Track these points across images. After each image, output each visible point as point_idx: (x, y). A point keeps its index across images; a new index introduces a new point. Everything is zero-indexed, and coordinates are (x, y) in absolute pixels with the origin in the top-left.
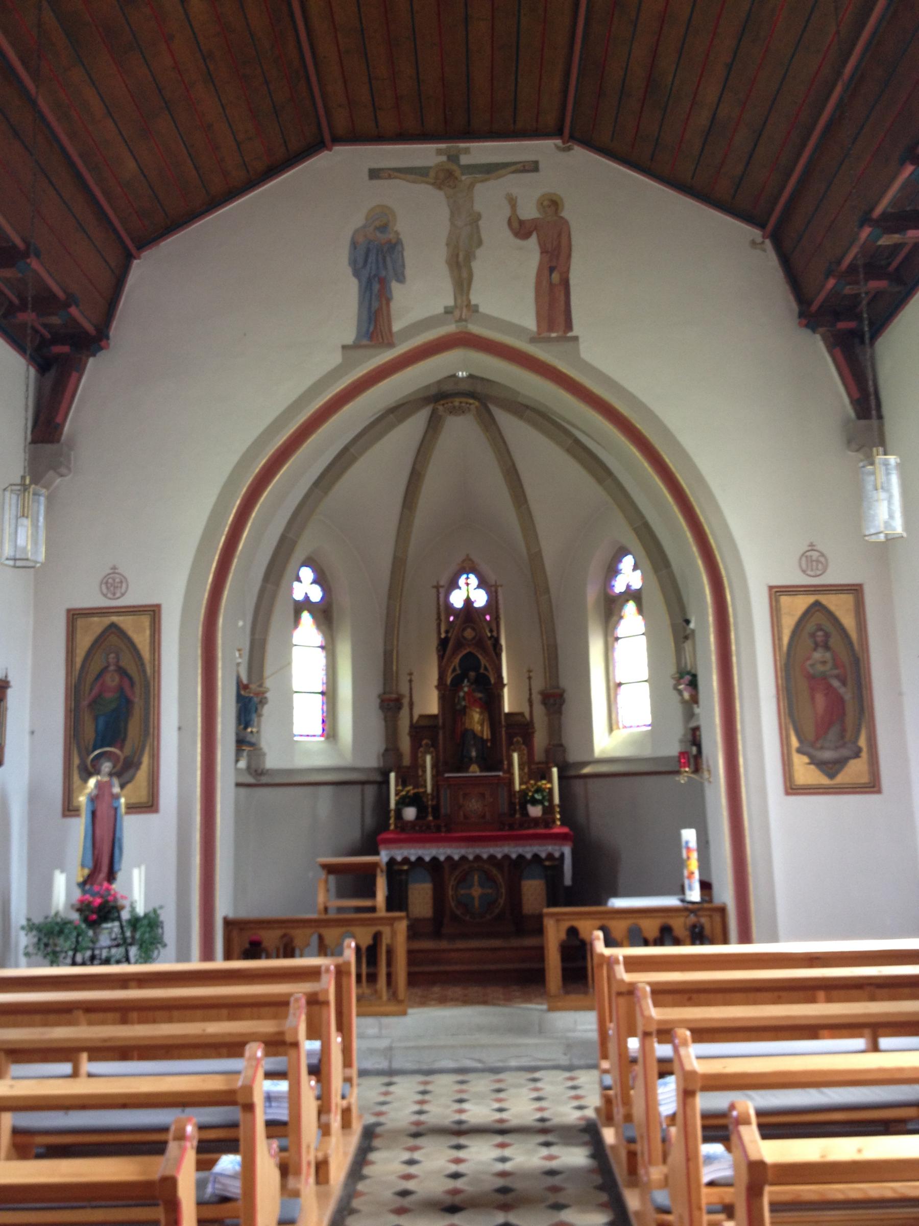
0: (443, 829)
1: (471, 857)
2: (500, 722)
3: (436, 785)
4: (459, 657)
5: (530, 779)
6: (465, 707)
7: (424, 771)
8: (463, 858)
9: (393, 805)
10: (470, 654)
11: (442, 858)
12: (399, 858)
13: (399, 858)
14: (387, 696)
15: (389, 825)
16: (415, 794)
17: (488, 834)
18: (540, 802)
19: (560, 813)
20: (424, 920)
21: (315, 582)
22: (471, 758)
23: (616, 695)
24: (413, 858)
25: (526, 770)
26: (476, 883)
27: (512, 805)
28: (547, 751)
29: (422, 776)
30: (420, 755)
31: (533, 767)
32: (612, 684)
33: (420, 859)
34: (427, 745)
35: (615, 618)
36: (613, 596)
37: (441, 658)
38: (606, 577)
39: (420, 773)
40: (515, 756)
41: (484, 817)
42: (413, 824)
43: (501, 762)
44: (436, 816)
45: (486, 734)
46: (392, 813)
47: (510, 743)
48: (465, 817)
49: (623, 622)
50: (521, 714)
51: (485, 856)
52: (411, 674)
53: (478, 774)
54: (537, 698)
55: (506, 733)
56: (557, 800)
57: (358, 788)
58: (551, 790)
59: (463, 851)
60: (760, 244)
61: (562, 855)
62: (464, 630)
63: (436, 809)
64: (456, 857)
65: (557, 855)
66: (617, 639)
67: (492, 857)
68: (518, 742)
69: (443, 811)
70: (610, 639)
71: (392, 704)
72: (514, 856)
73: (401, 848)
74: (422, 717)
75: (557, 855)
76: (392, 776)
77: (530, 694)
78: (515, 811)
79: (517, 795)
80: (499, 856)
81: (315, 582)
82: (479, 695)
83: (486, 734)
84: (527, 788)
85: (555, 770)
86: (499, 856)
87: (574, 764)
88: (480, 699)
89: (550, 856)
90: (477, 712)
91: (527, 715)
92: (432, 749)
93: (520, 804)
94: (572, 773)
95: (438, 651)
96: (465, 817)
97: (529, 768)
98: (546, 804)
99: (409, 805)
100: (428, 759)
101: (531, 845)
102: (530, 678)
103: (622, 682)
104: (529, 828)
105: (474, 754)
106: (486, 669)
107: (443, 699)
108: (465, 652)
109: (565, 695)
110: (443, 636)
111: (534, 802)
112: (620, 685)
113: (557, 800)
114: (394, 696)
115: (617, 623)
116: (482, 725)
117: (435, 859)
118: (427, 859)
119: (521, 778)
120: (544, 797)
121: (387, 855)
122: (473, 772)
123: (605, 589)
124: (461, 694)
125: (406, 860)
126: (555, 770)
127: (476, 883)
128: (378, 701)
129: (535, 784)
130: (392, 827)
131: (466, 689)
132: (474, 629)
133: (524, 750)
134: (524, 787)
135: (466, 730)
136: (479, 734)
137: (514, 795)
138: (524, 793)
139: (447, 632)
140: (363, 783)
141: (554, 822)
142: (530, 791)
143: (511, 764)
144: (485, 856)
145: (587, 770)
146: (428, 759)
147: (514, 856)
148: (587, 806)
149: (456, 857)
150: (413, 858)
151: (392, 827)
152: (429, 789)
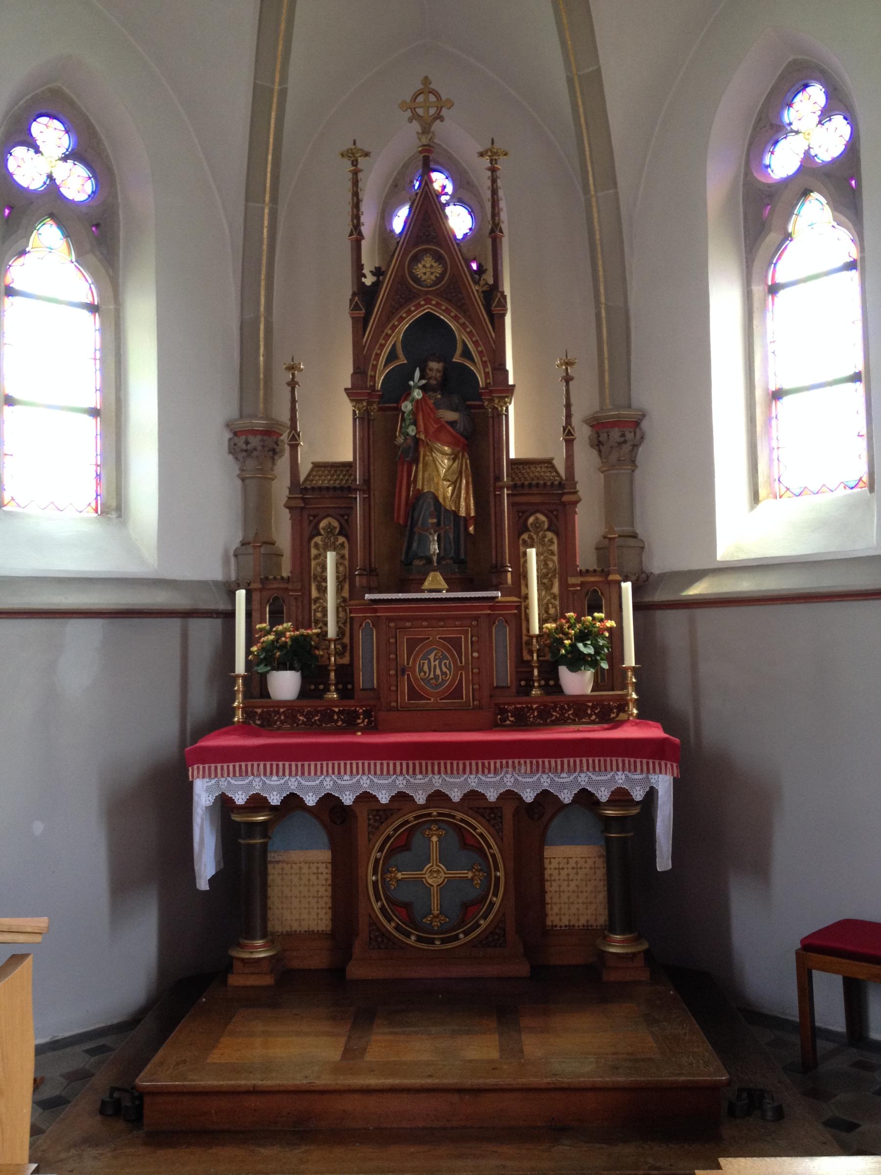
0: (361, 722)
1: (420, 798)
2: (498, 478)
3: (346, 624)
4: (405, 326)
5: (564, 609)
6: (417, 441)
7: (323, 590)
8: (401, 798)
9: (240, 667)
10: (429, 318)
11: (348, 799)
12: (240, 799)
13: (240, 799)
14: (245, 424)
15: (233, 711)
16: (294, 639)
17: (504, 428)
18: (592, 662)
19: (638, 688)
20: (311, 935)
21: (72, 156)
22: (429, 560)
23: (769, 419)
24: (275, 799)
25: (556, 590)
26: (435, 854)
27: (522, 666)
28: (603, 550)
29: (317, 600)
30: (314, 552)
31: (572, 580)
32: (759, 394)
33: (292, 801)
34: (330, 530)
35: (773, 237)
36: (769, 186)
37: (360, 324)
38: (750, 144)
39: (314, 594)
40: (532, 553)
41: (456, 693)
42: (290, 710)
43: (499, 569)
44: (345, 694)
45: (466, 506)
46: (240, 685)
47: (520, 527)
48: (414, 694)
49: (791, 247)
50: (548, 463)
51: (456, 796)
52: (292, 368)
53: (444, 594)
54: (583, 433)
55: (512, 505)
56: (630, 660)
57: (176, 622)
58: (617, 635)
59: (401, 783)
60: (479, 638)
61: (651, 794)
62: (416, 259)
63: (346, 674)
64: (384, 798)
65: (638, 795)
66: (774, 289)
67: (473, 796)
68: (537, 525)
69: (361, 681)
70: (758, 290)
71: (255, 441)
72: (529, 796)
73: (243, 774)
74: (318, 466)
75: (638, 795)
76: (241, 594)
77: (569, 416)
78: (530, 680)
79: (535, 645)
80: (492, 796)
81: (72, 156)
82: (450, 416)
83: (466, 506)
84: (559, 629)
85: (627, 587)
86: (492, 796)
87: (663, 577)
88: (452, 424)
89: (621, 797)
90: (444, 453)
91: (560, 465)
92: (341, 539)
93: (541, 665)
94: (660, 596)
95: (355, 307)
96: (414, 694)
97: (564, 585)
98: (605, 665)
99: (282, 666)
100: (331, 558)
101: (572, 770)
102: (568, 379)
103: (786, 386)
104: (562, 721)
105: (435, 548)
106: (466, 354)
107: (363, 420)
108: (417, 314)
109: (645, 424)
110: (369, 281)
111: (576, 661)
112: (777, 395)
113: (630, 660)
114: (260, 423)
115: (778, 248)
116: (456, 484)
117: (329, 801)
118: (311, 800)
119: (544, 607)
120: (598, 650)
121: (208, 790)
122: (431, 591)
123: (748, 173)
124: (407, 406)
125: (257, 803)
126: (627, 587)
127: (435, 854)
128: (227, 435)
129: (578, 620)
130: (238, 717)
131: (417, 394)
132: (438, 258)
133: (551, 542)
134: (551, 626)
135: (419, 494)
136: (450, 506)
137: (529, 643)
138: (550, 641)
139: (378, 272)
140: (187, 614)
141: (622, 707)
142: (566, 634)
143: (521, 576)
144: (456, 796)
145: (697, 590)
146: (331, 558)
147: (529, 796)
148: (694, 667)
149: (384, 798)
150: (275, 799)
151: (238, 717)
152: (332, 631)
